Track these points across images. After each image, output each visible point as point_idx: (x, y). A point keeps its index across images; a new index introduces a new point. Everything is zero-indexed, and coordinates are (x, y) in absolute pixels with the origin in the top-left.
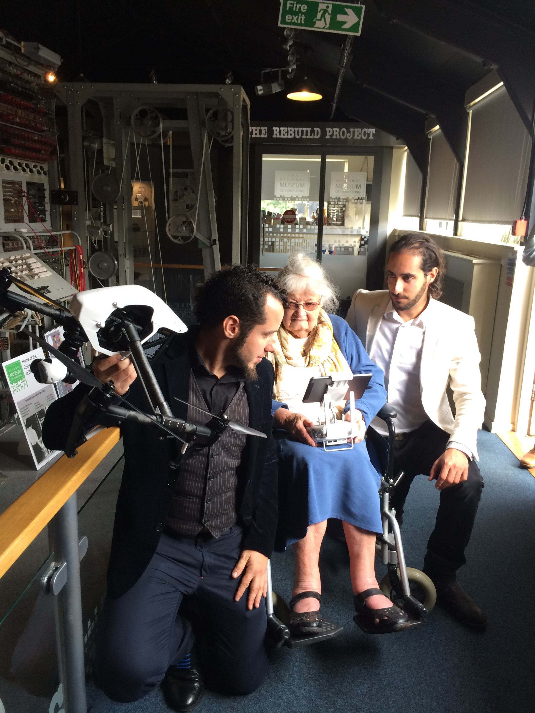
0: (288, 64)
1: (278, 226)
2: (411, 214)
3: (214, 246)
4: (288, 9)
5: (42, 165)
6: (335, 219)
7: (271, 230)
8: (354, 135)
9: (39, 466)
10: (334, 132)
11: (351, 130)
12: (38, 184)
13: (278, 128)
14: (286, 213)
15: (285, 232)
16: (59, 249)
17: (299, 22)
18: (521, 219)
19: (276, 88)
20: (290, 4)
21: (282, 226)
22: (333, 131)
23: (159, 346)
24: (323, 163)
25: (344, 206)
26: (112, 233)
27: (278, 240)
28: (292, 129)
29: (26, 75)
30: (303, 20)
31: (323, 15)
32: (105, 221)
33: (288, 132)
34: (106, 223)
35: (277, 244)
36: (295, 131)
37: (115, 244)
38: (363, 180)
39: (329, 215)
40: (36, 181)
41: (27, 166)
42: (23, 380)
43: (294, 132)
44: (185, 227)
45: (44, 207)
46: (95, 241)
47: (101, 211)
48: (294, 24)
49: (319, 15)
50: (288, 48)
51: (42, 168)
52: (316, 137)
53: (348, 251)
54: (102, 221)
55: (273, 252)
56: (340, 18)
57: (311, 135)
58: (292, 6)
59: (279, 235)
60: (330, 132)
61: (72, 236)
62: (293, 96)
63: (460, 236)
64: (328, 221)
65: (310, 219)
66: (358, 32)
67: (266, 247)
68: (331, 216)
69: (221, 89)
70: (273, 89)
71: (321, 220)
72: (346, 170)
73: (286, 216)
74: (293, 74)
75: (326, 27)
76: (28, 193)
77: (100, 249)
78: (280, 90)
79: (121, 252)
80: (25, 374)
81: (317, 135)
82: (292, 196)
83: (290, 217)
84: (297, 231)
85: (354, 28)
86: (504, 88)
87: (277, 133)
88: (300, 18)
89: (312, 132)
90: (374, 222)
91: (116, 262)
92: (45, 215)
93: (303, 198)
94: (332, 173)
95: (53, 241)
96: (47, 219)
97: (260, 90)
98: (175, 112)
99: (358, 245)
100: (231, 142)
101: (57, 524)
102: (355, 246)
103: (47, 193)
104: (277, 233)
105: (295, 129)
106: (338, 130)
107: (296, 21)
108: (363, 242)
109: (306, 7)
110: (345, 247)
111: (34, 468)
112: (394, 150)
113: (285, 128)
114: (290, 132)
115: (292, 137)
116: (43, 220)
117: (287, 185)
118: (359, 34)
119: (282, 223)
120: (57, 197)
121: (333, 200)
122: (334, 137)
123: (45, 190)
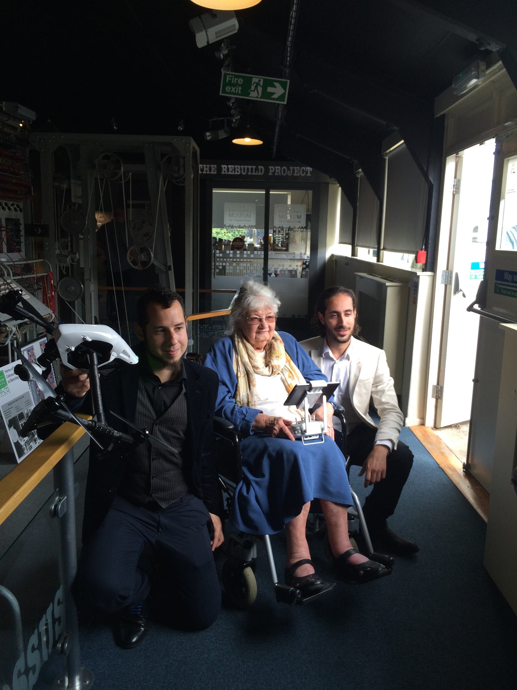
0: (232, 116)
1: (228, 252)
2: (345, 242)
3: (170, 272)
4: (227, 81)
6: (280, 245)
7: (221, 255)
9: (19, 461)
10: (276, 170)
11: (291, 168)
12: (15, 219)
13: (226, 166)
14: (236, 240)
15: (235, 257)
16: (38, 275)
18: (422, 249)
19: (222, 135)
20: (229, 77)
21: (231, 252)
22: (275, 169)
25: (287, 234)
26: (78, 261)
28: (239, 166)
29: (6, 129)
30: (240, 91)
32: (72, 250)
35: (227, 268)
37: (82, 272)
38: (302, 211)
40: (13, 217)
41: (6, 204)
42: (6, 387)
43: (241, 170)
44: (144, 255)
45: (20, 239)
46: (63, 267)
47: (68, 241)
49: (253, 88)
50: (231, 105)
51: (18, 206)
52: (260, 174)
53: (292, 274)
54: (69, 250)
55: (224, 275)
56: (270, 89)
57: (255, 172)
59: (228, 260)
60: (272, 169)
61: (43, 264)
63: (382, 262)
65: (257, 246)
66: (284, 101)
67: (217, 271)
68: (277, 243)
71: (267, 246)
72: (289, 202)
73: (236, 243)
75: (259, 97)
76: (6, 228)
77: (67, 275)
79: (86, 276)
81: (261, 172)
83: (239, 244)
84: (245, 256)
86: (405, 145)
89: (257, 169)
90: (314, 249)
91: (82, 286)
92: (20, 246)
94: (276, 205)
95: (28, 269)
97: (208, 136)
98: (135, 157)
99: (300, 269)
102: (297, 269)
103: (22, 228)
104: (227, 258)
106: (279, 168)
109: (242, 81)
112: (330, 185)
113: (233, 166)
114: (236, 169)
115: (239, 173)
116: (19, 251)
119: (232, 249)
120: (30, 231)
122: (276, 174)
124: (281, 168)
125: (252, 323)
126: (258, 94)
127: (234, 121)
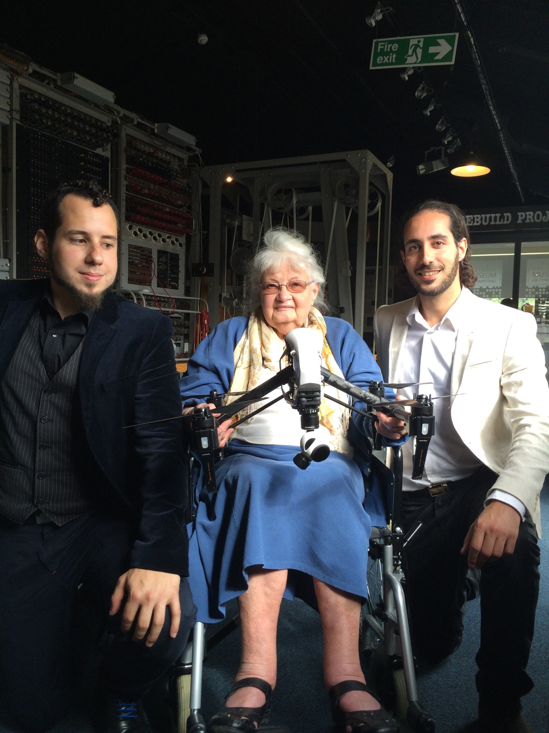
4: (379, 51)
10: (528, 216)
17: (390, 61)
19: (438, 166)
22: (526, 215)
28: (479, 216)
30: (394, 59)
31: (415, 51)
33: (474, 220)
43: (481, 219)
49: (410, 52)
52: (505, 222)
56: (432, 50)
57: (500, 221)
58: (383, 47)
60: (522, 216)
62: (457, 172)
66: (451, 61)
70: (434, 167)
75: (418, 62)
78: (443, 168)
81: (507, 220)
82: (481, 287)
85: (447, 57)
88: (391, 57)
89: (502, 217)
97: (422, 169)
105: (482, 215)
106: (531, 213)
107: (387, 62)
113: (471, 216)
114: (476, 220)
118: (453, 63)
120: (193, 271)
121: (530, 290)
122: (527, 221)
124: (534, 214)
125: (267, 293)
126: (417, 59)
127: (446, 143)
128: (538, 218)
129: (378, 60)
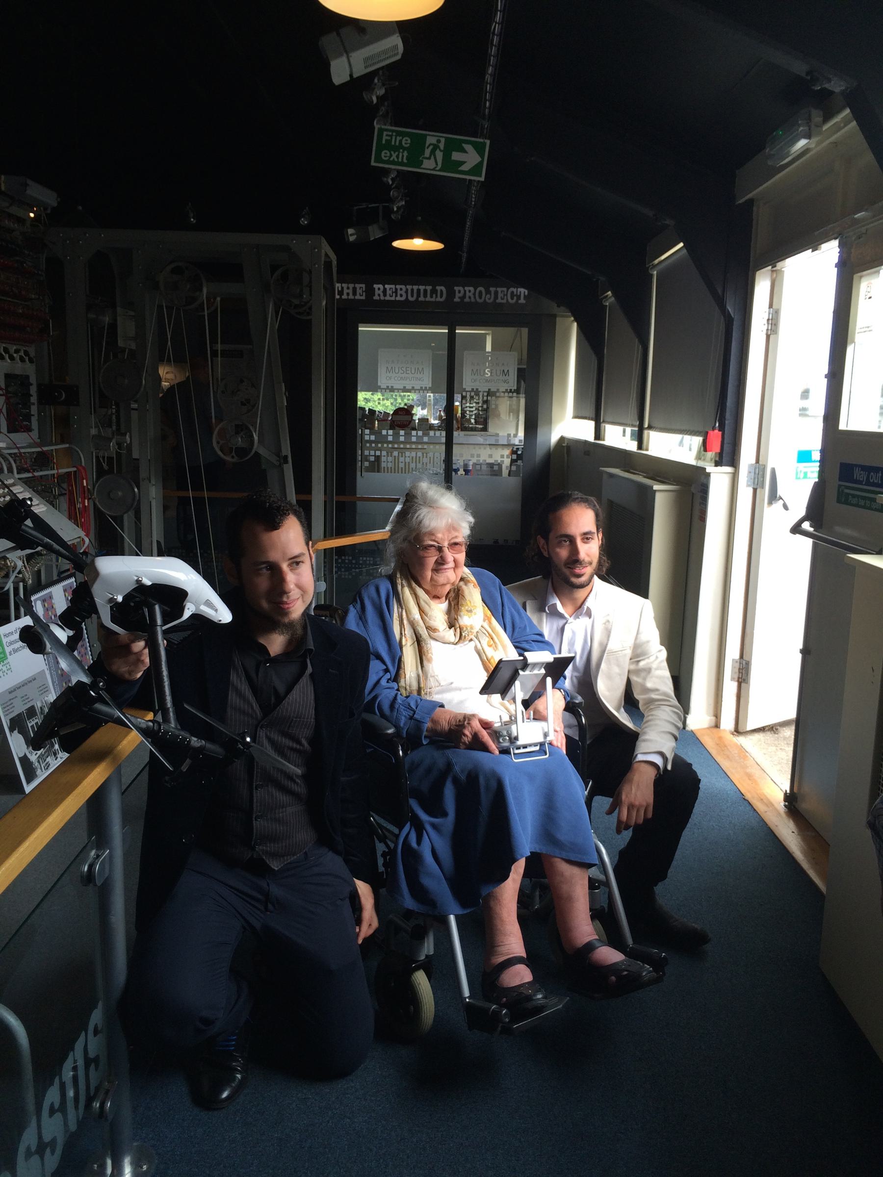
0: (392, 201)
1: (384, 432)
4: (384, 142)
5: (27, 348)
6: (473, 421)
7: (373, 438)
8: (496, 297)
9: (28, 789)
10: (466, 292)
13: (381, 286)
14: (398, 411)
15: (396, 440)
17: (400, 160)
18: (714, 429)
19: (375, 233)
21: (391, 432)
23: (189, 632)
24: (452, 336)
25: (486, 402)
27: (384, 453)
28: (403, 287)
29: (7, 222)
32: (118, 429)
34: (119, 432)
35: (383, 459)
36: (407, 290)
39: (463, 412)
40: (18, 372)
43: (406, 292)
44: (242, 437)
46: (104, 458)
47: (112, 414)
48: (393, 163)
49: (427, 153)
52: (439, 299)
53: (494, 469)
54: (114, 428)
55: (378, 471)
56: (456, 156)
57: (431, 297)
58: (389, 138)
59: (385, 445)
61: (69, 452)
63: (647, 450)
64: (462, 424)
66: (481, 176)
67: (367, 464)
68: (468, 417)
69: (292, 240)
71: (451, 422)
72: (489, 348)
73: (398, 418)
74: (400, 213)
77: (110, 471)
79: (143, 474)
80: (8, 654)
81: (441, 297)
83: (403, 418)
84: (414, 439)
85: (476, 170)
86: (685, 251)
87: (380, 292)
89: (434, 291)
90: (531, 427)
91: (136, 490)
92: (30, 422)
93: (423, 390)
94: (465, 353)
95: (43, 460)
96: (33, 427)
97: (351, 235)
98: (226, 269)
99: (507, 462)
100: (309, 314)
101: (96, 804)
103: (33, 390)
106: (472, 289)
108: (515, 457)
109: (409, 141)
110: (488, 464)
111: (21, 790)
113: (393, 286)
114: (399, 292)
116: (28, 429)
117: (397, 371)
120: (47, 396)
122: (467, 300)
123: (32, 385)
128: (480, 297)
129: (383, 154)
